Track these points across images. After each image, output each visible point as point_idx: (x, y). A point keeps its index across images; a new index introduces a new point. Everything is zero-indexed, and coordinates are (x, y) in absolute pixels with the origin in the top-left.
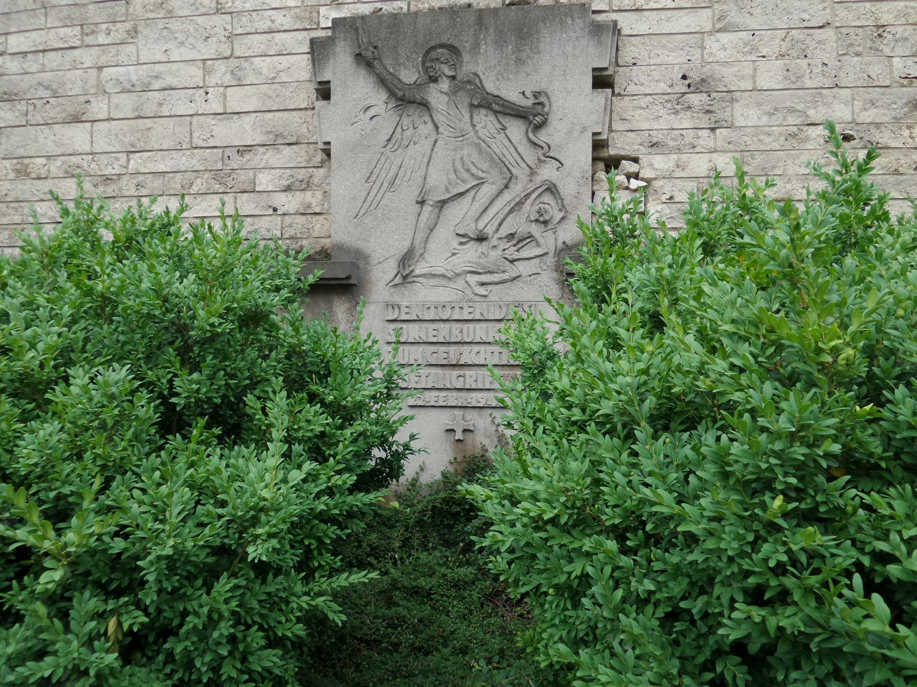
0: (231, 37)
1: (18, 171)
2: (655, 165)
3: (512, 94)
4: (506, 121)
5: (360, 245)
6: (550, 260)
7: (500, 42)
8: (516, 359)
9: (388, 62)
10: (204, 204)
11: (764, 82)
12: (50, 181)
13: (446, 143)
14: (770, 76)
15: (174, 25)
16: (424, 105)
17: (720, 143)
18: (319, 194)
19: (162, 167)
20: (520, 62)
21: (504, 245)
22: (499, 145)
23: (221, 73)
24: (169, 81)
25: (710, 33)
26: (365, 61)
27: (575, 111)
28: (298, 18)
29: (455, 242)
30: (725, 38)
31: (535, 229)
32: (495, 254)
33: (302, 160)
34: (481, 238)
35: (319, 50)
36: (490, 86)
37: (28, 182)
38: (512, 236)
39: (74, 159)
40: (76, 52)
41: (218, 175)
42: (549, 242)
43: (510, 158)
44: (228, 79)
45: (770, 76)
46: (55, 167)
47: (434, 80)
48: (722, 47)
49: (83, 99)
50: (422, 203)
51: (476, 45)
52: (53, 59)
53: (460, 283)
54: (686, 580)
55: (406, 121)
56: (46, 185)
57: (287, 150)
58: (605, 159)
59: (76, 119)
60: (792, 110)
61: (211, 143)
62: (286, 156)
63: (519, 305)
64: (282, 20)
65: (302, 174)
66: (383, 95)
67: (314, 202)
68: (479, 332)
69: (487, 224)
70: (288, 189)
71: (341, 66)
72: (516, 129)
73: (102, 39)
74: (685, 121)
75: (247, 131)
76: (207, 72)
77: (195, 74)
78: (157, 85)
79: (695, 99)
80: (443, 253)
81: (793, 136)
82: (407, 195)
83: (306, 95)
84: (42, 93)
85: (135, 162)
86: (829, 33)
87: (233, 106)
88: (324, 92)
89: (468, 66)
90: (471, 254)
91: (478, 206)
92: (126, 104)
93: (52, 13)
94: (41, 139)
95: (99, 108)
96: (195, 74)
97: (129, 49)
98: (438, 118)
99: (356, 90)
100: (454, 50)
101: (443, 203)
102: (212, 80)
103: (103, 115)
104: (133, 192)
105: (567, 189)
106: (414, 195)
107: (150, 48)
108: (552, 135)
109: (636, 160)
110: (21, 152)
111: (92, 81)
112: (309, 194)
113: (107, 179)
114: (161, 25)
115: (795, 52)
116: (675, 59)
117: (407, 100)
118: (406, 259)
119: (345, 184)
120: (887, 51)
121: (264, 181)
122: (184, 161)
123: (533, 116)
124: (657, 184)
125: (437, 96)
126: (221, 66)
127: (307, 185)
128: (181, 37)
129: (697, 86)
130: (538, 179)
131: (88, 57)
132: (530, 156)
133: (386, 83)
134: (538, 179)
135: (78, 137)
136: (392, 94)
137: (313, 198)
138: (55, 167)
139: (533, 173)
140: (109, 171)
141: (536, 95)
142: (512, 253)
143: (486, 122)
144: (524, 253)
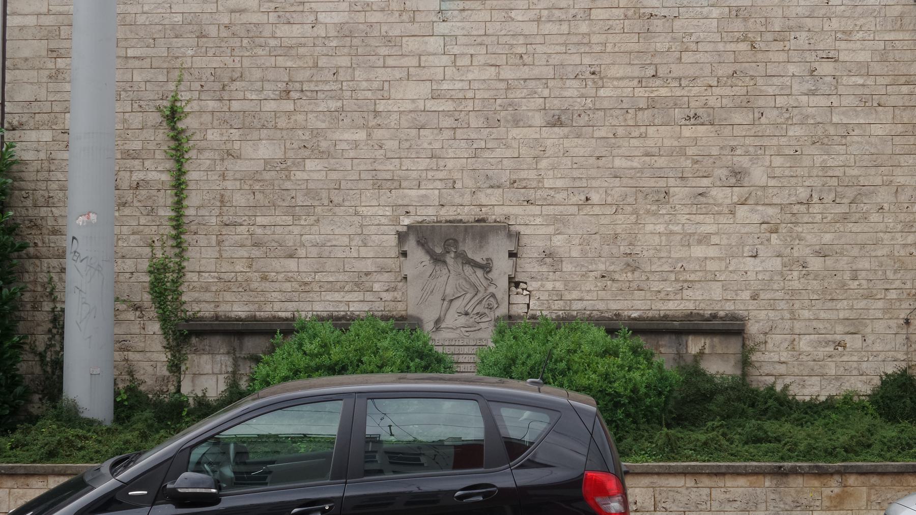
0: (361, 226)
2: (533, 285)
4: (476, 269)
5: (419, 315)
6: (493, 323)
7: (474, 239)
8: (34, 264)
9: (430, 244)
10: (350, 296)
11: (574, 254)
12: (277, 283)
13: (450, 279)
14: (575, 253)
15: (336, 219)
16: (445, 262)
17: (557, 278)
18: (400, 293)
19: (331, 279)
20: (481, 247)
21: (475, 317)
22: (473, 279)
23: (357, 241)
24: (334, 243)
25: (554, 235)
26: (422, 243)
27: (502, 266)
28: (391, 220)
29: (456, 315)
30: (559, 237)
31: (486, 311)
32: (472, 320)
34: (467, 314)
35: (402, 237)
36: (470, 255)
37: (268, 283)
38: (478, 314)
40: (290, 228)
41: (357, 284)
42: (492, 315)
43: (477, 283)
44: (360, 243)
45: (575, 253)
46: (281, 277)
47: (448, 252)
48: (558, 240)
51: (464, 239)
52: (279, 230)
53: (458, 331)
54: (280, 154)
55: (437, 268)
56: (277, 285)
57: (386, 275)
58: (514, 283)
59: (291, 256)
60: (583, 266)
61: (353, 270)
62: (386, 277)
63: (481, 339)
64: (384, 221)
65: (393, 285)
66: (428, 258)
68: (466, 350)
69: (469, 308)
70: (387, 290)
71: (411, 245)
72: (480, 273)
73: (303, 222)
74: (544, 269)
75: (369, 266)
76: (351, 240)
78: (329, 244)
79: (548, 260)
80: (453, 319)
81: (583, 275)
82: (437, 297)
83: (394, 252)
84: (274, 244)
86: (597, 236)
87: (363, 255)
88: (404, 254)
89: (461, 247)
90: (462, 320)
91: (465, 302)
92: (314, 252)
94: (274, 264)
95: (302, 252)
96: (346, 240)
98: (450, 268)
99: (417, 255)
101: (452, 300)
102: (353, 243)
105: (499, 296)
106: (440, 297)
107: (326, 228)
108: (493, 275)
109: (526, 283)
110: (264, 270)
111: (298, 241)
112: (396, 293)
113: (306, 284)
114: (330, 218)
116: (540, 244)
117: (438, 260)
118: (438, 322)
119: (413, 292)
120: (619, 243)
121: (376, 287)
122: (341, 277)
123: (486, 267)
124: (534, 293)
125: (450, 259)
126: (357, 238)
127: (395, 289)
129: (550, 256)
130: (488, 292)
131: (296, 230)
132: (485, 283)
134: (488, 292)
135: (292, 264)
136: (432, 257)
137: (398, 295)
139: (486, 289)
140: (306, 280)
141: (487, 259)
142: (478, 320)
143: (468, 270)
144: (483, 320)
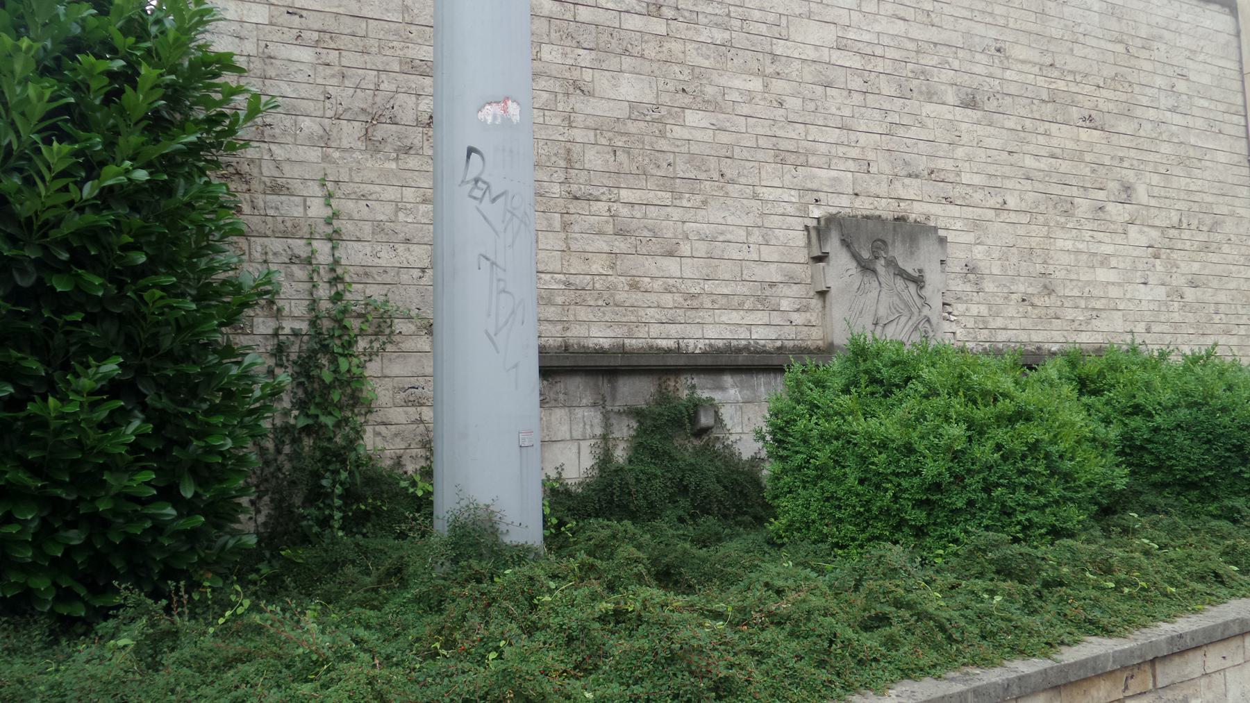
1: (631, 286)
3: (910, 268)
7: (903, 242)
9: (856, 246)
10: (752, 317)
15: (729, 202)
16: (874, 271)
20: (912, 253)
23: (756, 236)
24: (729, 237)
26: (846, 243)
30: (980, 247)
33: (803, 294)
36: (900, 264)
39: (671, 282)
40: (669, 209)
41: (759, 299)
44: (760, 240)
46: (657, 285)
47: (877, 258)
48: (979, 252)
49: (675, 241)
50: (876, 324)
51: (894, 242)
55: (866, 279)
56: (653, 297)
57: (795, 287)
59: (671, 254)
62: (795, 290)
66: (855, 264)
67: (813, 319)
70: (798, 310)
71: (833, 245)
72: (912, 288)
73: (685, 203)
74: (968, 287)
75: (773, 273)
76: (748, 234)
77: (741, 235)
78: (721, 238)
79: (971, 276)
84: (646, 233)
85: (708, 286)
86: (1014, 250)
87: (765, 257)
91: (900, 327)
92: (702, 249)
93: (651, 180)
94: (647, 264)
95: (685, 249)
96: (741, 235)
97: (704, 212)
98: (881, 279)
100: (884, 242)
102: (751, 240)
103: (688, 254)
104: (710, 306)
107: (714, 214)
108: (927, 292)
110: (634, 272)
111: (680, 230)
115: (1004, 258)
117: (866, 268)
121: (785, 304)
125: (880, 266)
128: (733, 210)
131: (676, 214)
132: (919, 302)
133: (856, 256)
135: (671, 266)
136: (859, 263)
138: (657, 285)
140: (692, 290)
143: (900, 282)
